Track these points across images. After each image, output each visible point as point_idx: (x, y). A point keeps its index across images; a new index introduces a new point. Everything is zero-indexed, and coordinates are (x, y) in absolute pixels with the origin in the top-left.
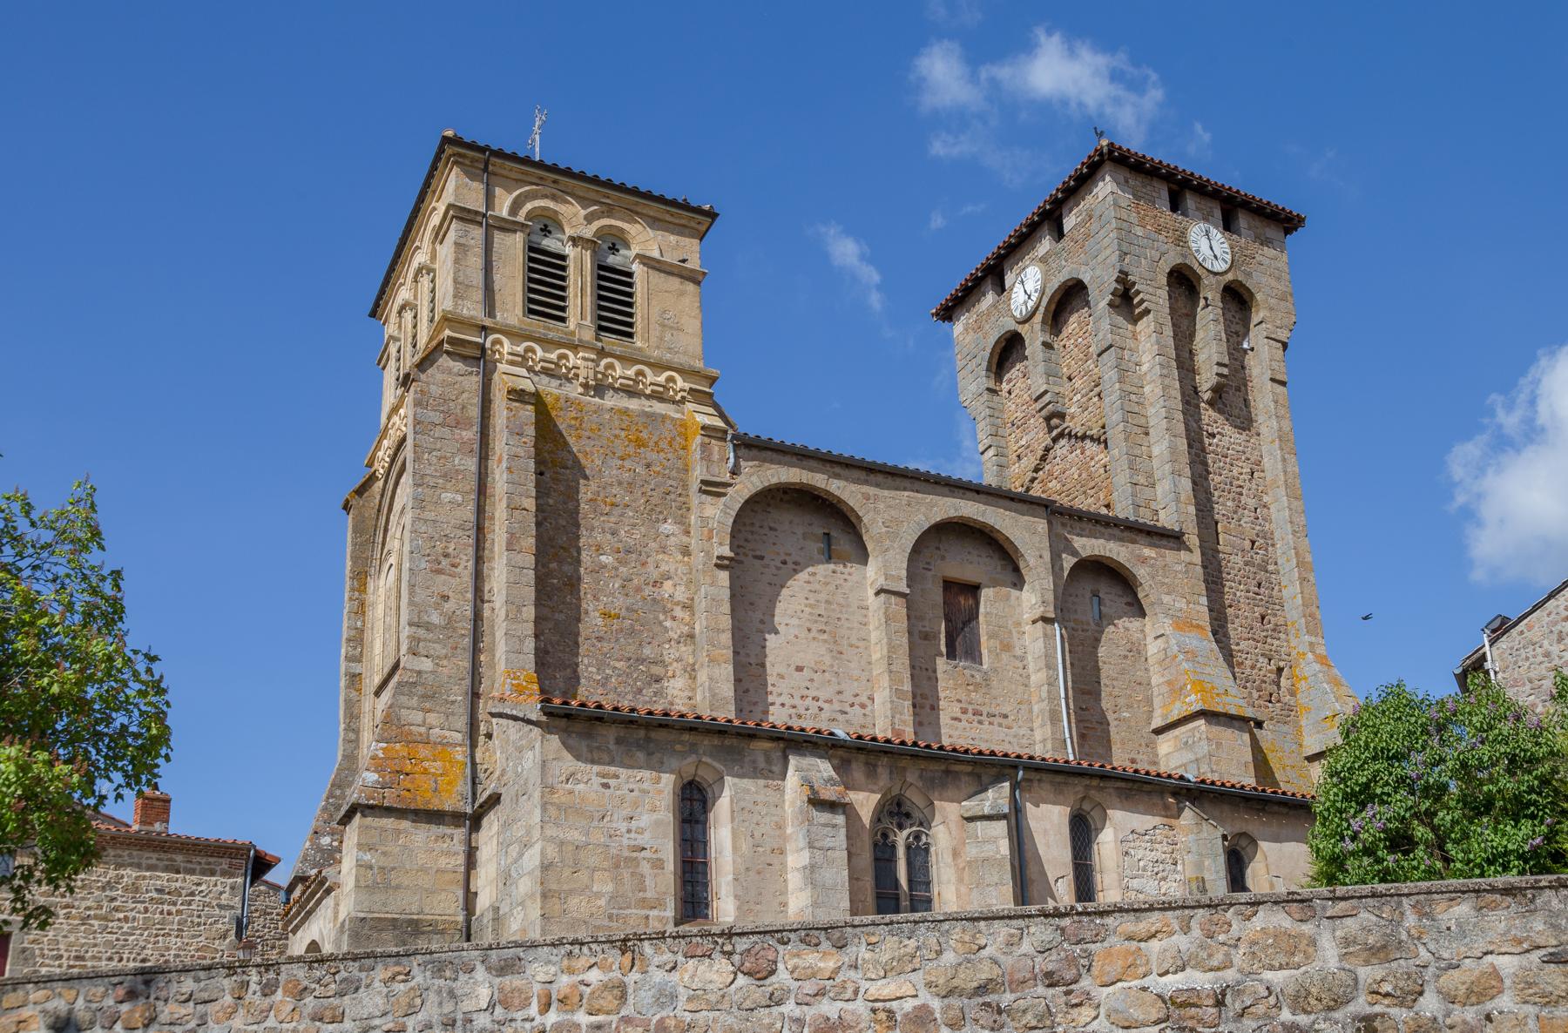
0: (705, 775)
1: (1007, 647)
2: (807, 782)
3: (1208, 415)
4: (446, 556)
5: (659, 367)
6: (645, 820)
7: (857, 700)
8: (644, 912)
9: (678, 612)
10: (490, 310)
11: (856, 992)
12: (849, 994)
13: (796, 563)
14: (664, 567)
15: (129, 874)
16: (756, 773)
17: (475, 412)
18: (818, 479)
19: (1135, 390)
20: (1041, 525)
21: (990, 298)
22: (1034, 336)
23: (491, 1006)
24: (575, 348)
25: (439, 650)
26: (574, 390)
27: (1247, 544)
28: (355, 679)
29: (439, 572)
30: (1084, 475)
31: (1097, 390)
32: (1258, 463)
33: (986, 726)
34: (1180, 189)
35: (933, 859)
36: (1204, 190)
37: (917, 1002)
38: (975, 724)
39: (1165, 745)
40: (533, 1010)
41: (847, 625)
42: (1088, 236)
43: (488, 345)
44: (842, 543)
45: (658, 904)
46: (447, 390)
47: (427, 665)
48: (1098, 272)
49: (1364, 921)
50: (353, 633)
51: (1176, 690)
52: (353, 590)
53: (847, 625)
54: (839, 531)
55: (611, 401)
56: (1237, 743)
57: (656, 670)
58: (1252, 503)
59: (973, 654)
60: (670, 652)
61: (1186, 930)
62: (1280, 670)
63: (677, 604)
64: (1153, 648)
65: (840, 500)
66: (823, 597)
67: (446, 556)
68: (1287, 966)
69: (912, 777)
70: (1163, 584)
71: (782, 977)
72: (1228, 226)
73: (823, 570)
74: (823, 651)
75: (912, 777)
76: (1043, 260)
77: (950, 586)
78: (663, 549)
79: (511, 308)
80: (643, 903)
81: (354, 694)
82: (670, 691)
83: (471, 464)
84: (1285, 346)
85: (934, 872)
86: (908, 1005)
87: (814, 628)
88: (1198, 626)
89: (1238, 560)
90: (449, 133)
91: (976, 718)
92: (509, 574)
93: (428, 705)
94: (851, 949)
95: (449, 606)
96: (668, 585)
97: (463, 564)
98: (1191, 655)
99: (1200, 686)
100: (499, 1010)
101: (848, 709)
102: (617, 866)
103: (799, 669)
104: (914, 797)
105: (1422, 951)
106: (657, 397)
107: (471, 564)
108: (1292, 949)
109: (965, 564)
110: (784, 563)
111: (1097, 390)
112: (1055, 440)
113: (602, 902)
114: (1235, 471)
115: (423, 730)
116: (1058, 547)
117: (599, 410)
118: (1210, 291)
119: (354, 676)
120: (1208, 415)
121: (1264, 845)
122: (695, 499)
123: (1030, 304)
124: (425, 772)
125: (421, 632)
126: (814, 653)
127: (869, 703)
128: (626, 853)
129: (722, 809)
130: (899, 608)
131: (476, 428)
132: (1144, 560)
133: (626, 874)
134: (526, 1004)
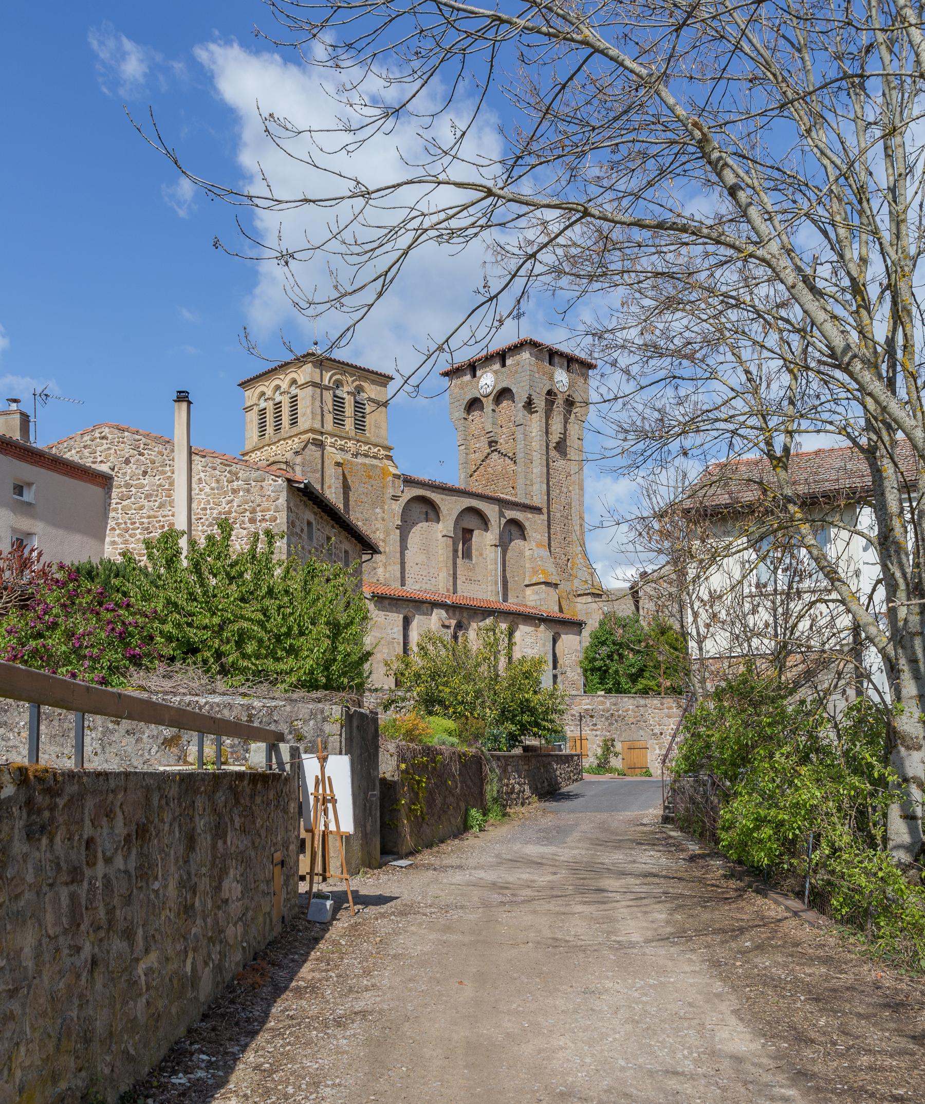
0: (410, 614)
1: (481, 554)
2: (440, 619)
3: (553, 453)
5: (376, 445)
6: (395, 630)
17: (319, 466)
20: (496, 508)
21: (468, 377)
22: (488, 404)
24: (349, 439)
26: (348, 456)
34: (552, 355)
36: (562, 355)
39: (529, 591)
42: (516, 372)
44: (432, 515)
49: (613, 700)
51: (535, 572)
54: (430, 510)
55: (360, 460)
56: (553, 594)
58: (565, 490)
64: (528, 553)
69: (465, 614)
72: (568, 370)
75: (465, 614)
76: (496, 372)
78: (376, 519)
79: (329, 426)
89: (558, 515)
98: (541, 558)
99: (544, 572)
104: (465, 621)
106: (375, 457)
108: (603, 703)
109: (471, 522)
116: (502, 515)
117: (358, 463)
118: (560, 400)
122: (389, 501)
126: (421, 558)
129: (414, 624)
130: (450, 541)
132: (528, 519)
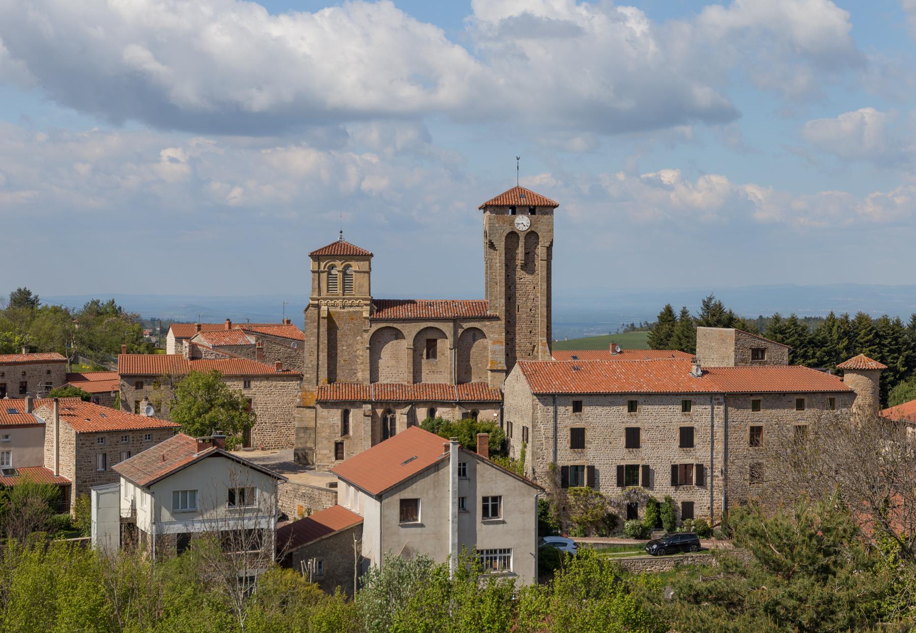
15: (274, 383)
16: (357, 408)
18: (391, 325)
24: (338, 299)
26: (338, 310)
54: (398, 335)
55: (345, 310)
58: (532, 297)
59: (435, 356)
60: (358, 367)
62: (534, 346)
73: (395, 342)
77: (428, 341)
92: (324, 356)
104: (392, 408)
120: (520, 273)
121: (481, 411)
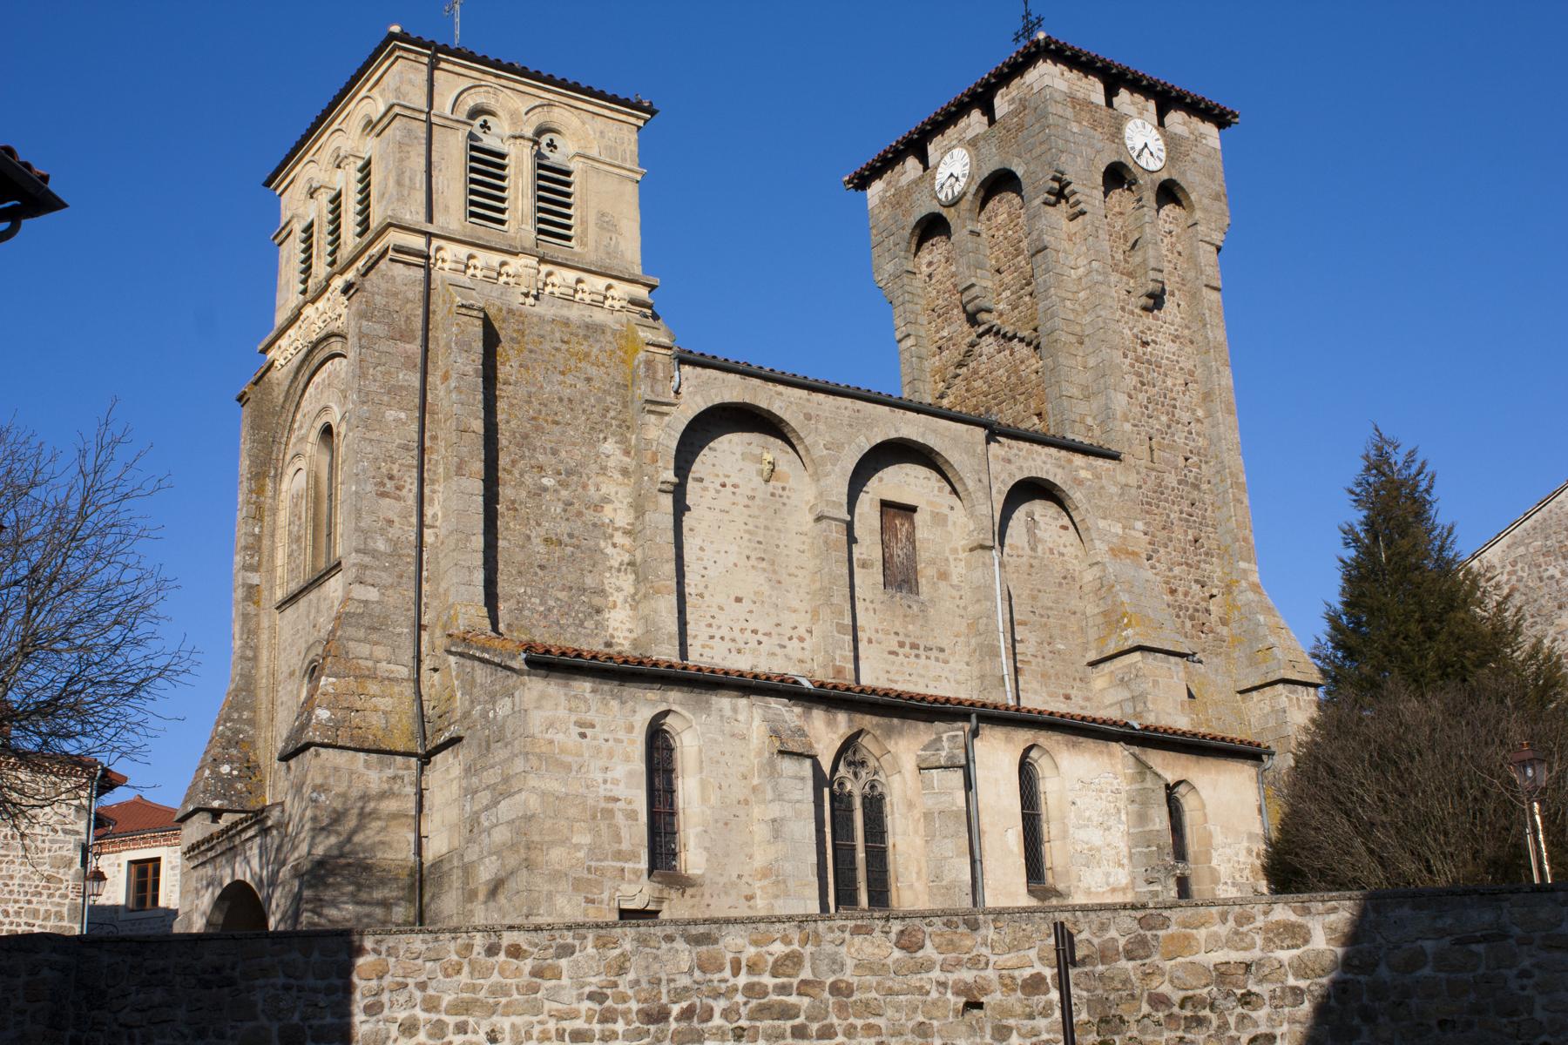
4: (391, 478)
6: (620, 771)
7: (795, 634)
8: (619, 864)
9: (619, 538)
10: (430, 219)
11: (987, 964)
12: (982, 965)
13: (735, 486)
14: (604, 490)
17: (418, 324)
19: (1070, 296)
23: (690, 972)
25: (386, 578)
27: (1181, 462)
28: (252, 592)
29: (383, 495)
30: (1013, 379)
31: (1029, 289)
32: (1191, 373)
33: (923, 660)
35: (888, 809)
37: (1034, 971)
38: (912, 659)
40: (727, 973)
41: (786, 552)
42: (1021, 127)
43: (432, 253)
45: (634, 856)
46: (391, 300)
47: (373, 594)
48: (1032, 167)
50: (250, 540)
52: (251, 491)
53: (786, 552)
57: (597, 601)
61: (1224, 920)
63: (616, 529)
65: (781, 420)
66: (761, 522)
67: (391, 478)
68: (1293, 947)
70: (1099, 507)
71: (929, 951)
74: (762, 579)
76: (973, 144)
80: (619, 855)
81: (251, 609)
82: (612, 624)
83: (415, 380)
84: (1219, 249)
85: (889, 821)
86: (1027, 973)
87: (753, 556)
88: (1134, 553)
90: (396, 29)
91: (915, 652)
92: (454, 501)
93: (374, 636)
94: (983, 931)
95: (393, 532)
96: (608, 508)
97: (408, 486)
100: (697, 974)
101: (786, 642)
102: (594, 818)
103: (739, 600)
105: (1379, 938)
107: (415, 488)
110: (724, 485)
111: (1029, 289)
112: (980, 336)
113: (581, 854)
114: (1169, 383)
115: (370, 664)
119: (251, 587)
123: (957, 189)
124: (376, 710)
125: (367, 560)
127: (807, 636)
128: (603, 804)
131: (419, 341)
133: (603, 825)
134: (721, 969)
